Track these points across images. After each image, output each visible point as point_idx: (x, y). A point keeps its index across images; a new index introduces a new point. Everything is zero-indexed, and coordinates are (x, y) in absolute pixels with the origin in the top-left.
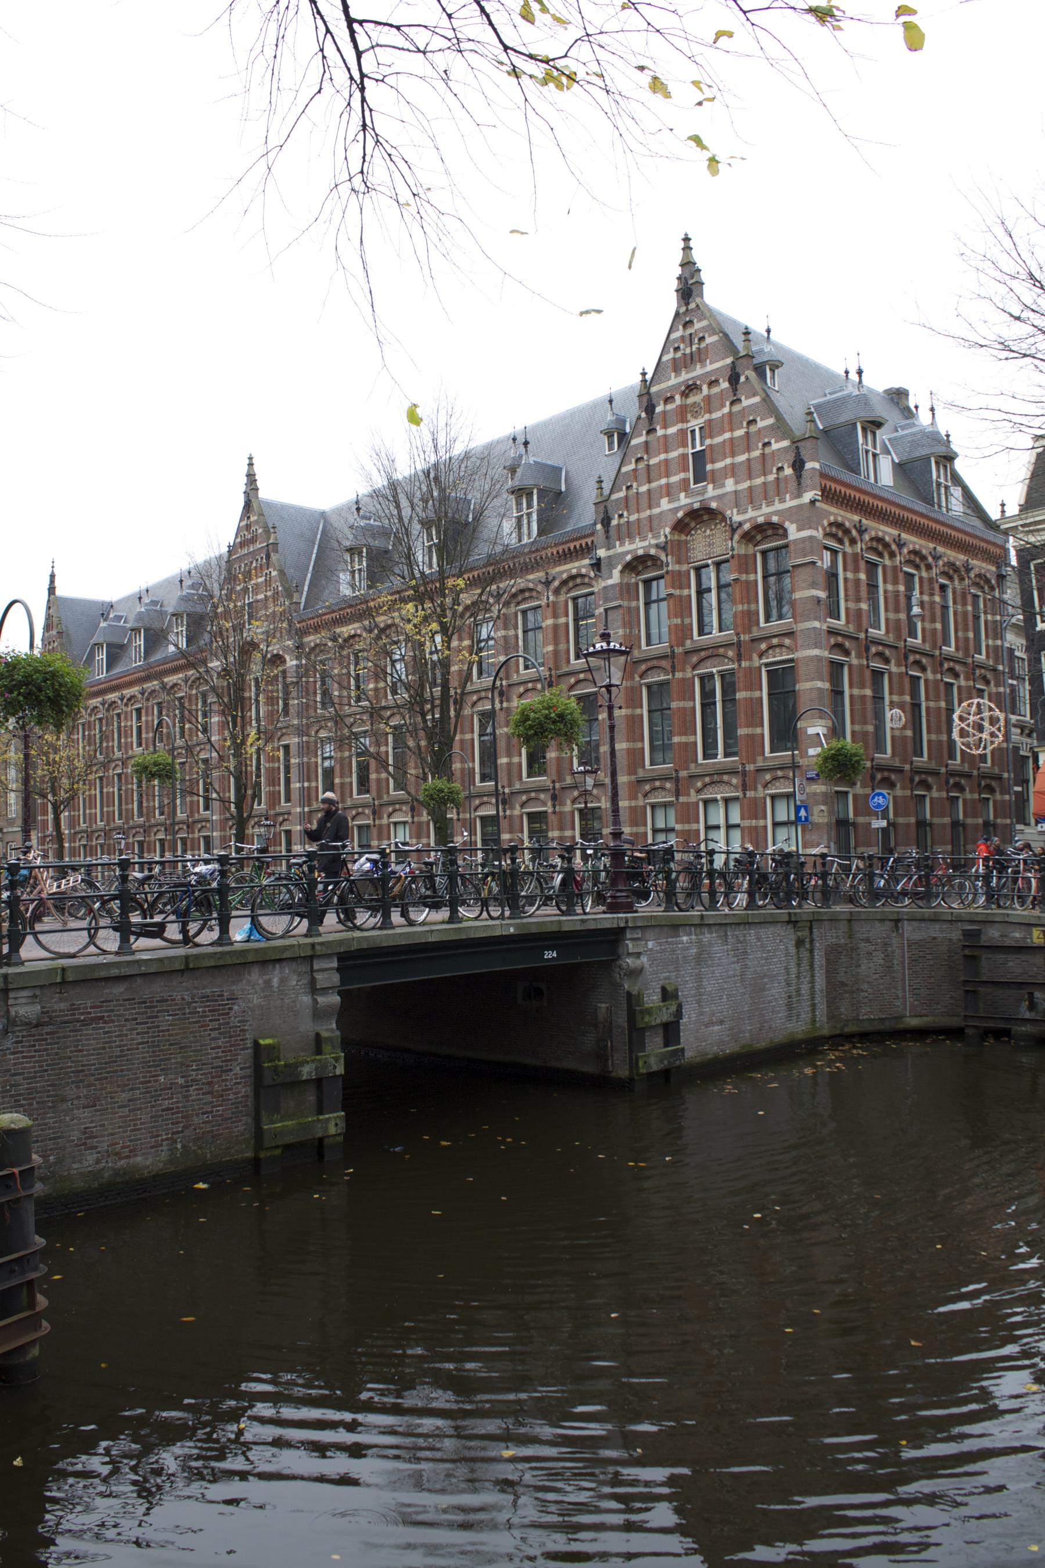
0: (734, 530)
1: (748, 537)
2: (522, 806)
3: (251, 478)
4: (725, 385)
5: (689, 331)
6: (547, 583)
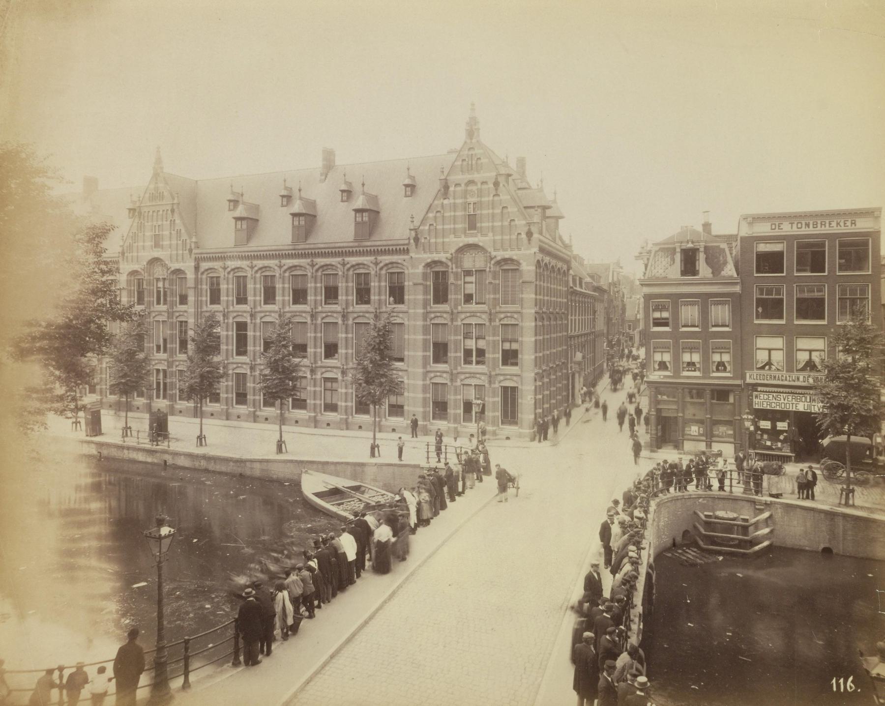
0: (492, 259)
1: (498, 263)
2: (462, 380)
3: (159, 161)
4: (491, 186)
5: (470, 153)
6: (376, 264)
